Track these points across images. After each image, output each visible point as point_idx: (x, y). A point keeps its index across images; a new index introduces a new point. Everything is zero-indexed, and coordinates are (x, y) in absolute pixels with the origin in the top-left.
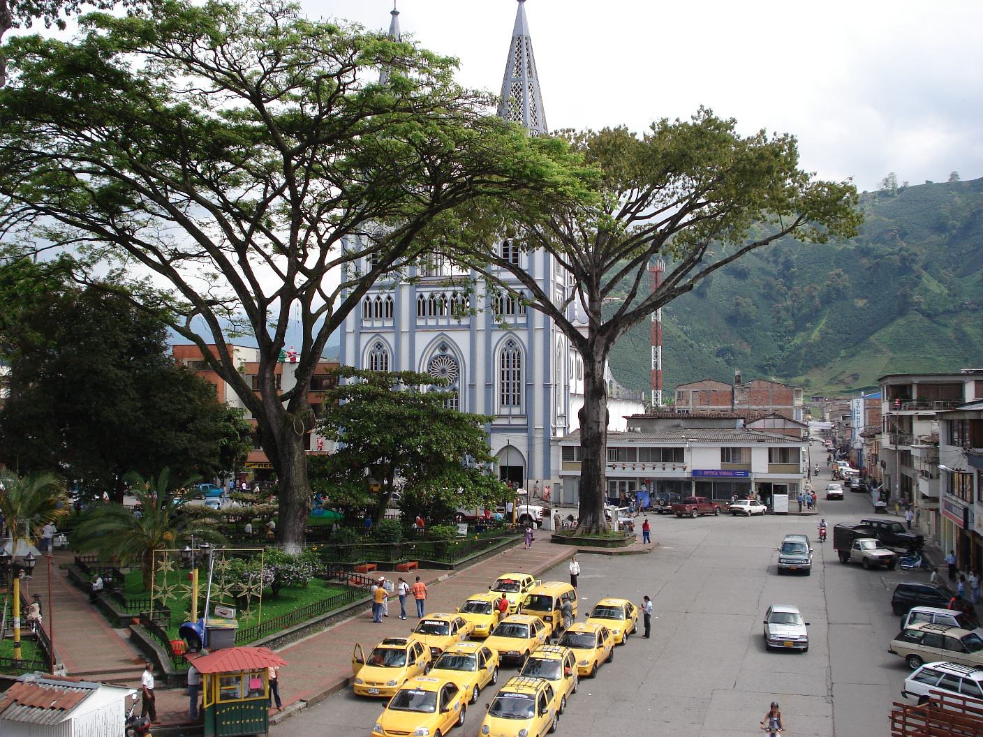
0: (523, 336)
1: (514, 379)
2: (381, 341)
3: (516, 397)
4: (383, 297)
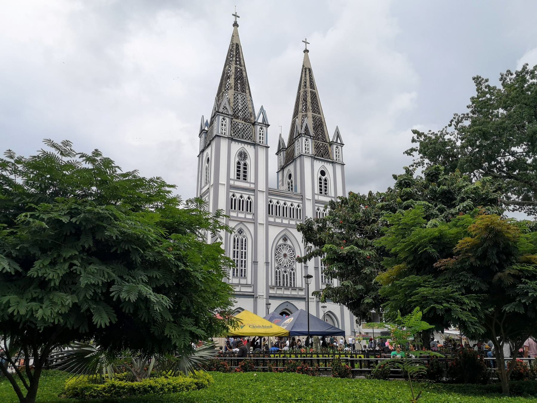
0: (251, 227)
1: (238, 252)
2: (243, 227)
3: (243, 262)
4: (245, 197)
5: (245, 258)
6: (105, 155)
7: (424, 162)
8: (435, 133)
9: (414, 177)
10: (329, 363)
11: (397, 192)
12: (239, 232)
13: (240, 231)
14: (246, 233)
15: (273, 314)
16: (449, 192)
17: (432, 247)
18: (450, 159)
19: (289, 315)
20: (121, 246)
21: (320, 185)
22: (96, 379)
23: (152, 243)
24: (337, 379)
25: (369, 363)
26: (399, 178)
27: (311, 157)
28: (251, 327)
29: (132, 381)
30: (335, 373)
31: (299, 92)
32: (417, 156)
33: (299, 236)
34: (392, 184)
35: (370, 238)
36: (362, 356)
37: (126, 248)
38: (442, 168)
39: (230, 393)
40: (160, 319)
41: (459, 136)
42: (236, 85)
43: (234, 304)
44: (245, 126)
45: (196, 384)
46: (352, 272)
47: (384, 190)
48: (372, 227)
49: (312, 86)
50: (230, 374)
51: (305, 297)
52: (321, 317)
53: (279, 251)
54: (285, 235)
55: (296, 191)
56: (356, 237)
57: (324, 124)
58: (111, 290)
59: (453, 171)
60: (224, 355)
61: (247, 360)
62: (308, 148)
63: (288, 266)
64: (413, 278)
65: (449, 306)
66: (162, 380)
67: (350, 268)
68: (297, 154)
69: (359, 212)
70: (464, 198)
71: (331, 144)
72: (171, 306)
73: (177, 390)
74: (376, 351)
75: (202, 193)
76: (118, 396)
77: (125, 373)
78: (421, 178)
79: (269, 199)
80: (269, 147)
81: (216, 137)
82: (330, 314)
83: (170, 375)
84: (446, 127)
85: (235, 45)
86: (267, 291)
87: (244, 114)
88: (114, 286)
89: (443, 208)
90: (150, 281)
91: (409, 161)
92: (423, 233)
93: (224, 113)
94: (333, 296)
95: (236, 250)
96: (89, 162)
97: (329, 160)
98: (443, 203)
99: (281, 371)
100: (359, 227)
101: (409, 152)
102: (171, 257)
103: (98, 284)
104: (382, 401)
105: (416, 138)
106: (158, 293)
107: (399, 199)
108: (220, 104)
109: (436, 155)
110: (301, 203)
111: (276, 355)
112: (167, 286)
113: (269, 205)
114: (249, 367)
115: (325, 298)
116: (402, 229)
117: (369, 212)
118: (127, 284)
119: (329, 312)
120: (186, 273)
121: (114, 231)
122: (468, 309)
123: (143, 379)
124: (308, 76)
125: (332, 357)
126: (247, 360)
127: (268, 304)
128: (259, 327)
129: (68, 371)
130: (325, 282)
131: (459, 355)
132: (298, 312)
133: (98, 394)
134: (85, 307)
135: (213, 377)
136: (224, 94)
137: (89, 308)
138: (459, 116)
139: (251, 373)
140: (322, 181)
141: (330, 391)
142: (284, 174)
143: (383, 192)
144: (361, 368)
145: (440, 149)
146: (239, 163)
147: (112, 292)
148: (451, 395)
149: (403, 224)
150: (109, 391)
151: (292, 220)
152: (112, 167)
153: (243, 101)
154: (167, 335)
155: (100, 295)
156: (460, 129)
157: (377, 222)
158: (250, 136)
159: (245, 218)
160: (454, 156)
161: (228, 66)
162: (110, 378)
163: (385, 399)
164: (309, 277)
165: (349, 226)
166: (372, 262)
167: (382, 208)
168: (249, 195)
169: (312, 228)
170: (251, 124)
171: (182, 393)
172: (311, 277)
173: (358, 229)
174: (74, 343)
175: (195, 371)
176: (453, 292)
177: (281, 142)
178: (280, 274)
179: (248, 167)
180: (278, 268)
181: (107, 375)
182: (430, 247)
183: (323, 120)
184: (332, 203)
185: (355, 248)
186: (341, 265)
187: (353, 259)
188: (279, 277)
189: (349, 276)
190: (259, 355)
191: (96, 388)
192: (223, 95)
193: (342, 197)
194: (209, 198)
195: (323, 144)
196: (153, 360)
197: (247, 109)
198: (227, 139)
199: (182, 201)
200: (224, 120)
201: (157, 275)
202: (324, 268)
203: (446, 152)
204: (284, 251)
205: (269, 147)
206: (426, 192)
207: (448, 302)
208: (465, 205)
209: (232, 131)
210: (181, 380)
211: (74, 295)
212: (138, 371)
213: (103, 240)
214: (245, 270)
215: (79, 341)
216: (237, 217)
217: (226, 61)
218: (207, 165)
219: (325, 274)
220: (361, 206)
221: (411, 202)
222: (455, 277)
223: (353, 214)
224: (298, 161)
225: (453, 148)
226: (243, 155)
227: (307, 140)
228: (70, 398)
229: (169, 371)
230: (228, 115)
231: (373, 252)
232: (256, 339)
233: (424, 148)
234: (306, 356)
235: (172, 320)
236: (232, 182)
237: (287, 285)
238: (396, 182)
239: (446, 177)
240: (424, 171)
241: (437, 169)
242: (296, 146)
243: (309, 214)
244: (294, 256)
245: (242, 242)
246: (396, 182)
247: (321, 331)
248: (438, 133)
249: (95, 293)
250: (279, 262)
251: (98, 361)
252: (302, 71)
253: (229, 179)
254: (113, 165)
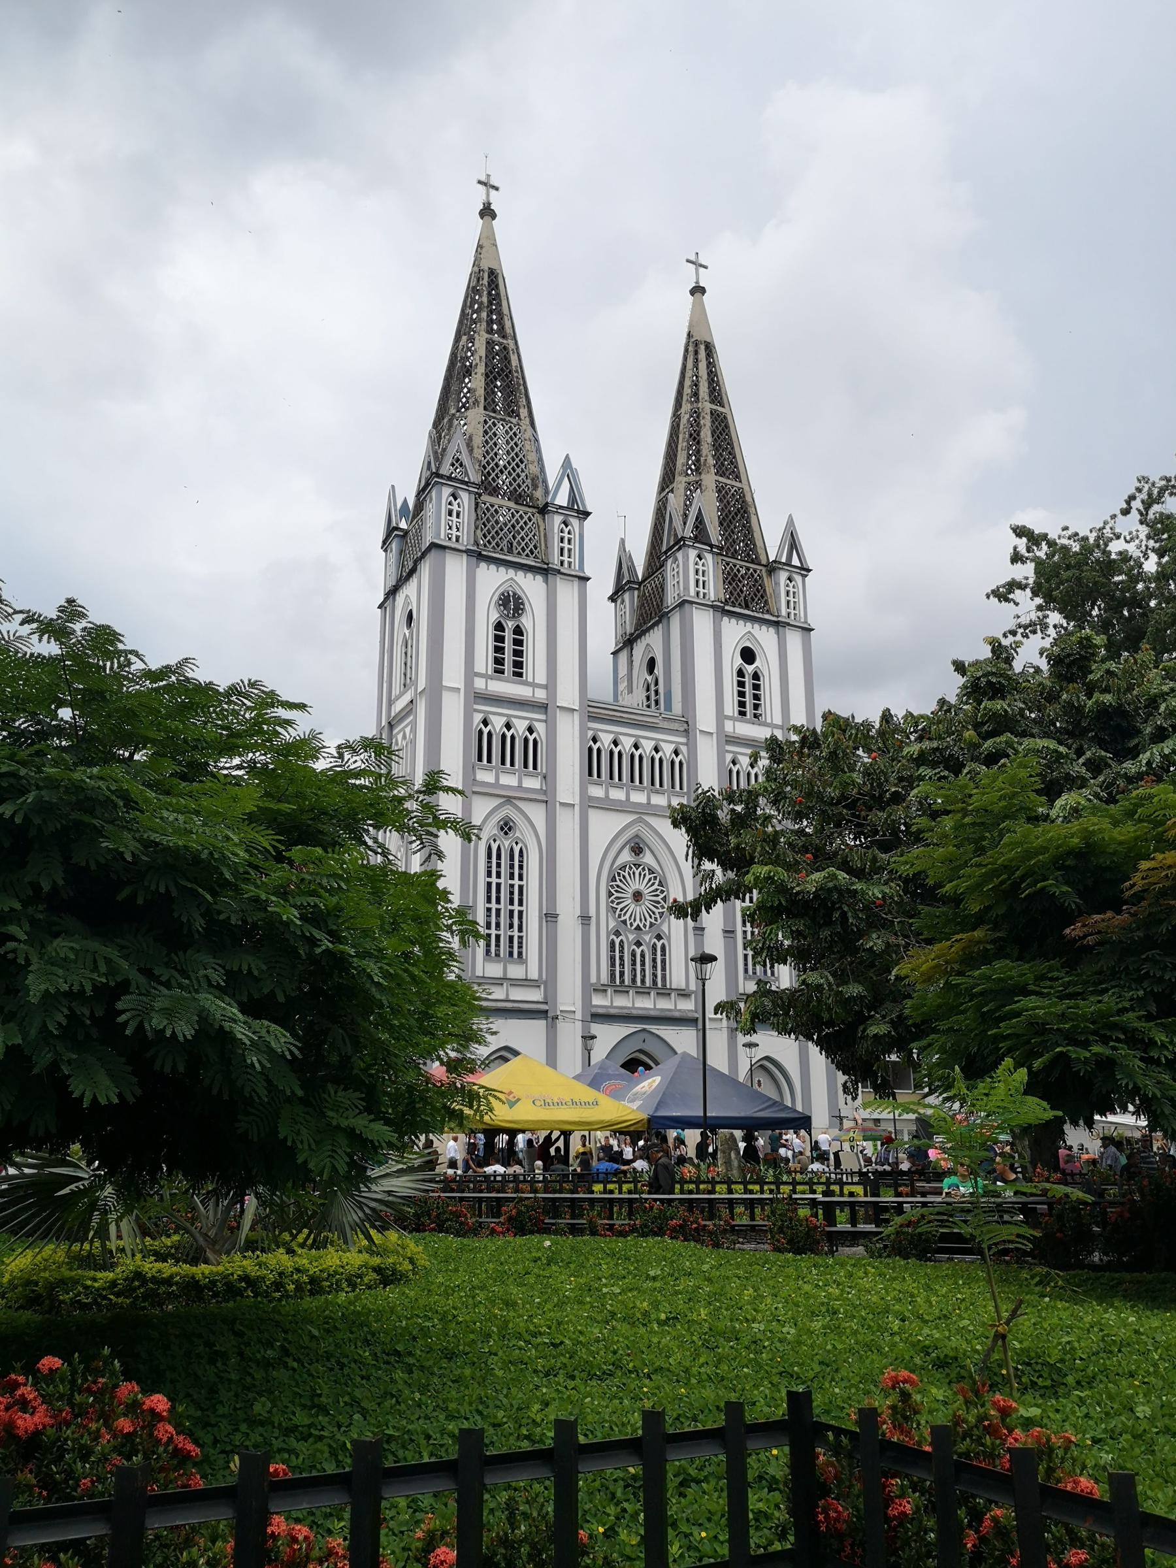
0: (537, 814)
1: (498, 885)
4: (520, 727)
5: (521, 904)
6: (97, 616)
7: (1048, 620)
8: (1081, 535)
9: (1018, 666)
10: (763, 1209)
11: (965, 712)
12: (502, 829)
13: (506, 824)
14: (522, 830)
15: (602, 1066)
16: (1119, 711)
17: (1060, 878)
18: (1126, 613)
19: (649, 1067)
20: (146, 884)
21: (739, 692)
22: (90, 1254)
23: (235, 873)
24: (782, 1257)
25: (878, 1213)
26: (972, 669)
27: (712, 606)
28: (537, 1103)
29: (194, 1262)
30: (778, 1241)
31: (676, 416)
32: (1027, 605)
33: (679, 840)
34: (952, 687)
35: (886, 847)
36: (859, 1189)
37: (162, 890)
38: (1099, 640)
39: (473, 1297)
40: (263, 1092)
41: (1151, 543)
42: (489, 393)
43: (489, 1038)
44: (517, 516)
45: (378, 1270)
46: (830, 947)
47: (926, 707)
48: (889, 816)
49: (717, 395)
50: (476, 1243)
51: (696, 1015)
52: (742, 1075)
53: (619, 883)
54: (637, 836)
55: (669, 707)
56: (844, 843)
57: (752, 510)
58: (120, 1005)
59: (1134, 648)
60: (459, 1184)
61: (526, 1202)
62: (704, 582)
63: (645, 926)
64: (1004, 969)
65: (1108, 1052)
66: (279, 1259)
67: (825, 933)
68: (671, 599)
69: (852, 770)
70: (1165, 729)
71: (772, 568)
72: (296, 1052)
73: (321, 1288)
74: (902, 1173)
75: (393, 714)
76: (153, 1305)
77: (176, 1238)
78: (1038, 670)
79: (590, 734)
80: (588, 579)
81: (433, 551)
82: (768, 1067)
83: (302, 1246)
84: (1114, 517)
85: (486, 275)
86: (587, 1000)
87: (514, 480)
88: (128, 997)
89: (1102, 759)
90: (232, 986)
91: (1001, 618)
92: (1040, 835)
93: (455, 479)
94: (775, 1015)
95: (494, 880)
96: (49, 638)
97: (767, 617)
98: (1102, 745)
99: (622, 1234)
100: (853, 815)
101: (1003, 594)
102: (292, 914)
103: (82, 991)
104: (911, 1323)
105: (1022, 550)
106: (256, 1018)
107: (972, 732)
108: (444, 450)
109: (1083, 601)
110: (682, 744)
111: (610, 1186)
112: (281, 999)
113: (590, 750)
114: (531, 1220)
115: (753, 1022)
116: (974, 824)
117: (882, 771)
118: (165, 991)
119: (767, 1058)
120: (339, 962)
121: (125, 841)
122: (1166, 1057)
123: (224, 1257)
124: (703, 365)
125: (771, 1191)
126: (526, 1202)
127: (588, 1038)
128: (560, 1103)
129: (12, 1232)
130: (754, 973)
131: (1141, 1191)
132: (676, 1060)
133: (95, 1300)
134: (43, 1059)
135: (426, 1248)
136: (456, 422)
137: (55, 1060)
138: (1153, 484)
139: (535, 1238)
140: (746, 679)
141: (760, 1293)
142: (634, 658)
143: (922, 713)
144: (854, 1225)
145: (1095, 583)
146: (499, 627)
147: (123, 1012)
148: (1112, 1306)
149: (977, 810)
150: (128, 1291)
151: (657, 792)
152: (119, 653)
153: (512, 443)
154: (286, 1139)
155: (88, 1022)
156: (1156, 521)
157: (904, 800)
158: (531, 546)
159: (520, 786)
160: (1137, 601)
161: (464, 338)
162: (129, 1255)
163: (920, 1317)
164: (706, 959)
165: (823, 812)
166: (889, 917)
167: (921, 759)
168: (532, 719)
169: (715, 817)
170: (534, 510)
171: (336, 1297)
172: (713, 959)
173: (848, 821)
174: (23, 1154)
175: (373, 1232)
176: (1123, 1011)
177: (623, 564)
178: (622, 951)
179: (528, 639)
180: (617, 934)
181: (121, 1243)
182: (1056, 879)
183: (748, 499)
184: (774, 747)
185: (842, 875)
186: (799, 924)
187: (833, 909)
188: (621, 958)
189: (823, 957)
190: (561, 1186)
191: (89, 1283)
192: (450, 426)
193: (803, 726)
194: (414, 731)
195: (748, 569)
196: (251, 1202)
197: (523, 466)
198: (465, 556)
199: (324, 747)
200: (456, 499)
201: (252, 966)
202: (753, 933)
203: (1114, 591)
204: (635, 885)
205: (588, 579)
206: (1051, 711)
207: (1105, 1040)
208: (1167, 751)
209: (479, 531)
210: (332, 1259)
211: (12, 1025)
212: (212, 1233)
213: (93, 867)
214: (520, 938)
215: (39, 1149)
216: (497, 784)
217: (461, 322)
218: (407, 632)
219: (754, 949)
220: (860, 752)
221: (1006, 742)
222: (1127, 967)
223: (835, 776)
224: (675, 621)
225: (1134, 579)
226: (511, 603)
228: (17, 1310)
229: (300, 1232)
230: (466, 483)
231: (893, 889)
232: (554, 1137)
233: (1048, 580)
234: (698, 1188)
235: (300, 1093)
236: (479, 684)
237: (643, 981)
238: (961, 680)
239: (1112, 666)
240: (1047, 650)
241: (1086, 643)
242: (669, 574)
243: (709, 778)
244: (664, 899)
245: (512, 858)
246: (961, 680)
247: (743, 1114)
248: (1088, 534)
249: (72, 1017)
250: (620, 916)
251: (93, 1206)
252: (686, 350)
253: (470, 673)
254: (120, 646)
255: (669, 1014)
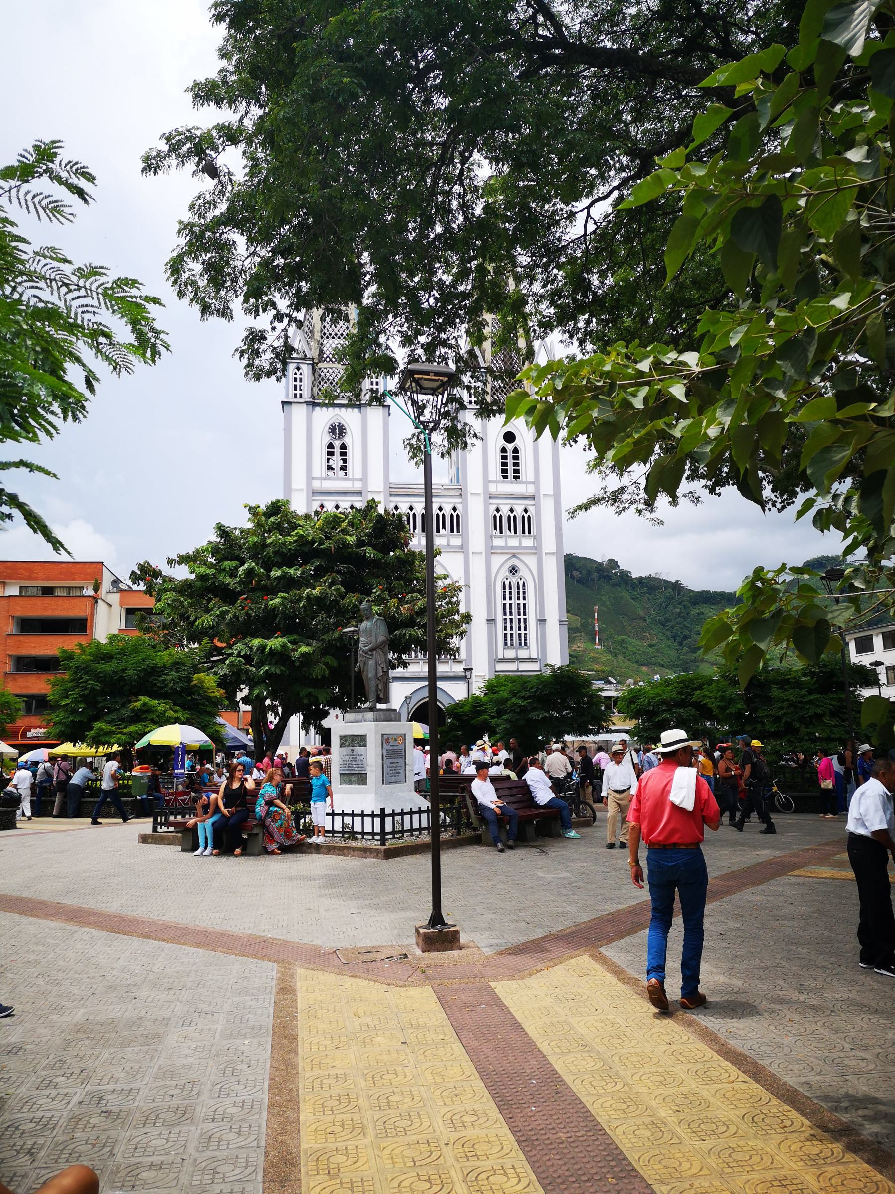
0: (531, 561)
3: (508, 621)
5: (525, 614)
12: (511, 571)
13: (513, 568)
14: (523, 572)
226: (338, 430)
227: (298, 369)
245: (518, 588)
253: (486, 481)
255: (445, 674)
